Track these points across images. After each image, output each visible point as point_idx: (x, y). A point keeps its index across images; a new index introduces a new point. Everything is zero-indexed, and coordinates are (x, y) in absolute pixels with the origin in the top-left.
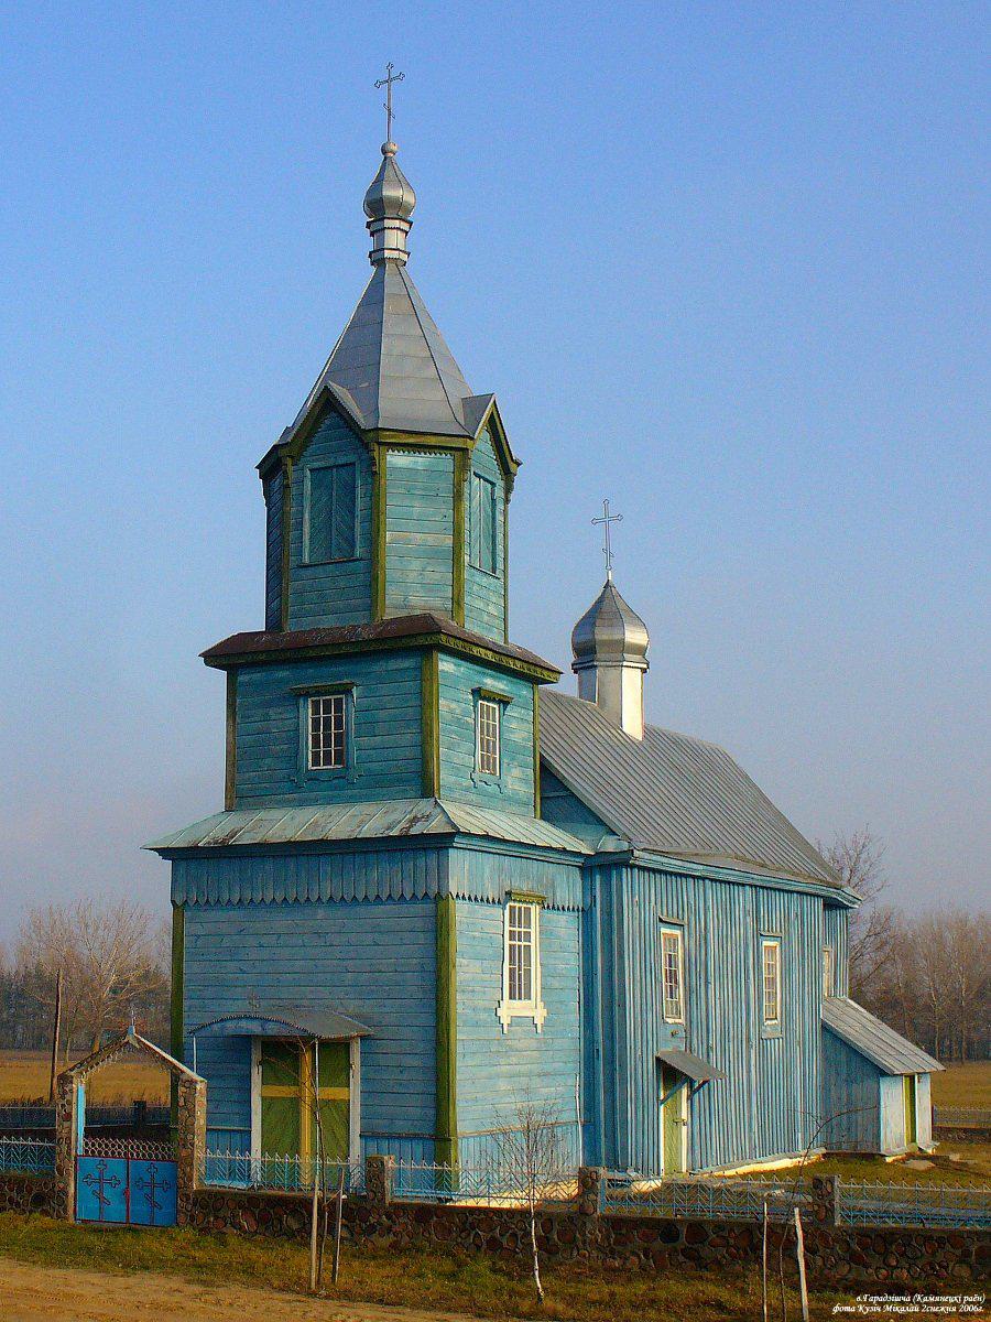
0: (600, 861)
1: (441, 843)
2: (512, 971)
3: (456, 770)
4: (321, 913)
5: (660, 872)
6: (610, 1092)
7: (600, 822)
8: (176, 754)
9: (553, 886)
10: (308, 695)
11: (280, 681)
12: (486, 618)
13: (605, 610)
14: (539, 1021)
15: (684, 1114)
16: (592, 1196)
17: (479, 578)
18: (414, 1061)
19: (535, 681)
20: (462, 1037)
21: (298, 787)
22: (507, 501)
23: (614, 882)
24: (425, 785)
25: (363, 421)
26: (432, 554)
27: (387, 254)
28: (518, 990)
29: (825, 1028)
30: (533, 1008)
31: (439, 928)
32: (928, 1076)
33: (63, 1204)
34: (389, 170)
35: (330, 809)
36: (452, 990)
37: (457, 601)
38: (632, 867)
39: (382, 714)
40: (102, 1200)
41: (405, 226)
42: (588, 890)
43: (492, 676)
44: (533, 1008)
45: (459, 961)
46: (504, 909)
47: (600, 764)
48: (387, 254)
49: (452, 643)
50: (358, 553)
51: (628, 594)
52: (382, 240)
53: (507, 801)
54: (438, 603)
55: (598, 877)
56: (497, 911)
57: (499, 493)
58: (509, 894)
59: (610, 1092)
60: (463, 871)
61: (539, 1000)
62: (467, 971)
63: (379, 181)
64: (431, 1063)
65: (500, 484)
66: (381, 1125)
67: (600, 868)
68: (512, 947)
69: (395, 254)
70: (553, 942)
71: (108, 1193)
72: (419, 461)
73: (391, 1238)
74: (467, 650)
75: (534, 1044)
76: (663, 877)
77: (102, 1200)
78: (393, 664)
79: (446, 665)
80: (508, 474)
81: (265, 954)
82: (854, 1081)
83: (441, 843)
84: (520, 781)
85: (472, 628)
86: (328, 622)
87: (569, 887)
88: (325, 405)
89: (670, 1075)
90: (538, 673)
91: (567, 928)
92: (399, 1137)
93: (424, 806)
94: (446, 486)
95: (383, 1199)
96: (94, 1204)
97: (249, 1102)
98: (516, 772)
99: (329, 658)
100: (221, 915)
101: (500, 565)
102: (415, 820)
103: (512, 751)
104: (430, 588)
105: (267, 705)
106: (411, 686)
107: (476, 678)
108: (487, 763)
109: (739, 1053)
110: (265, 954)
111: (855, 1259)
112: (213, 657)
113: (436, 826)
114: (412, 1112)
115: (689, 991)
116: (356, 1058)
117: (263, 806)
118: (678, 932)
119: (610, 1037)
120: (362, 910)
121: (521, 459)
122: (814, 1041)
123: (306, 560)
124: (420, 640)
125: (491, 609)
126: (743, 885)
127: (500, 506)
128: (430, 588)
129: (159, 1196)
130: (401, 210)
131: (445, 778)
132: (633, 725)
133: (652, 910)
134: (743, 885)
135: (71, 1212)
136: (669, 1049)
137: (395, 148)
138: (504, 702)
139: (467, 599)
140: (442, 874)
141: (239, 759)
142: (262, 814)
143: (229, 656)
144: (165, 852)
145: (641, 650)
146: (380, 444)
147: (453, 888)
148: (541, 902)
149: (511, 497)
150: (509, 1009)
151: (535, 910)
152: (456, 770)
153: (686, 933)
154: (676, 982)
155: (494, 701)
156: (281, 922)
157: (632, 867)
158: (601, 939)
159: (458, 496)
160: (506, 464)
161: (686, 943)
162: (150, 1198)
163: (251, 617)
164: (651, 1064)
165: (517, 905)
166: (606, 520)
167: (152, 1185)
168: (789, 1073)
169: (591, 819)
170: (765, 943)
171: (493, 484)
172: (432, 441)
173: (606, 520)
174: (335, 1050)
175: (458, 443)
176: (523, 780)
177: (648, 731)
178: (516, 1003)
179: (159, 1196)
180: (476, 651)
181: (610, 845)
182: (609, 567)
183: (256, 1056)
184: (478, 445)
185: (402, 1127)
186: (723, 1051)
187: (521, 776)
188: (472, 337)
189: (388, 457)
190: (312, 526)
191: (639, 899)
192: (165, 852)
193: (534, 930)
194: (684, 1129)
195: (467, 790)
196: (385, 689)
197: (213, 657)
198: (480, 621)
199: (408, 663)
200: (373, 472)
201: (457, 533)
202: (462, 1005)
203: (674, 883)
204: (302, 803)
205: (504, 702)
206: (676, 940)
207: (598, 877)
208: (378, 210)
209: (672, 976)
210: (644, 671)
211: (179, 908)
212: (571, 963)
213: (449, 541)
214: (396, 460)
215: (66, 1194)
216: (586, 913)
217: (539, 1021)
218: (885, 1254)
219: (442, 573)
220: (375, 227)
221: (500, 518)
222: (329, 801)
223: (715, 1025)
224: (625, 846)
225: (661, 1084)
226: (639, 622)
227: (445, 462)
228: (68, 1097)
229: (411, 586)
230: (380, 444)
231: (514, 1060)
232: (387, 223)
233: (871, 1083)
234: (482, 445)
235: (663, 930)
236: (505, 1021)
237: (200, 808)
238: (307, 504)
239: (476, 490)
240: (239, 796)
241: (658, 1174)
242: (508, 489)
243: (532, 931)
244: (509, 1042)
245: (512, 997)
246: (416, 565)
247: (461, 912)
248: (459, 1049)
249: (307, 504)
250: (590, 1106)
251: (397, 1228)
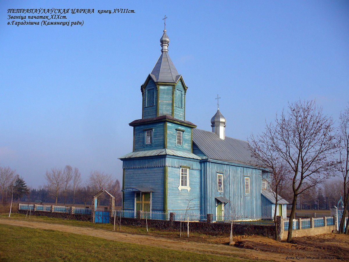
0: (203, 161)
1: (164, 156)
2: (182, 181)
3: (171, 143)
4: (146, 170)
5: (217, 163)
6: (205, 204)
7: (204, 154)
8: (125, 143)
9: (192, 165)
10: (146, 131)
11: (142, 128)
12: (179, 116)
13: (217, 115)
14: (189, 190)
15: (223, 209)
16: (172, 218)
17: (178, 109)
18: (160, 196)
19: (193, 128)
20: (169, 192)
21: (145, 147)
22: (185, 94)
23: (206, 165)
24: (164, 146)
25: (155, 80)
26: (168, 104)
27: (163, 50)
28: (184, 183)
29: (262, 195)
30: (188, 188)
31: (164, 172)
32: (286, 205)
33: (92, 219)
34: (164, 35)
35: (149, 151)
36: (166, 183)
37: (173, 113)
38: (209, 162)
39: (158, 134)
40: (99, 219)
41: (167, 45)
42: (201, 166)
43: (180, 127)
44: (188, 188)
45: (168, 178)
46: (180, 169)
47: (211, 143)
48: (163, 50)
49: (169, 120)
50: (154, 105)
51: (221, 112)
52: (163, 48)
53: (184, 150)
54: (169, 113)
55: (203, 164)
56: (178, 169)
57: (183, 93)
58: (181, 166)
59: (205, 204)
60: (169, 162)
61: (189, 186)
62: (170, 180)
63: (162, 38)
64: (163, 196)
65: (183, 91)
66: (155, 208)
67: (203, 162)
68: (182, 176)
69: (165, 50)
70: (193, 176)
71: (100, 218)
72: (166, 87)
73: (141, 225)
74: (173, 122)
75: (187, 194)
76: (246, 168)
77: (99, 219)
78: (160, 125)
79: (169, 124)
80: (185, 90)
81: (137, 177)
82: (267, 205)
83: (164, 156)
84: (188, 146)
85: (176, 117)
86: (150, 117)
87: (197, 166)
88: (149, 78)
89: (218, 202)
90: (193, 126)
91: (197, 174)
92: (158, 210)
93: (164, 150)
94: (171, 92)
95: (140, 218)
96: (97, 219)
97: (134, 202)
98: (187, 144)
99: (150, 125)
100: (131, 170)
101: (183, 106)
102: (160, 153)
103: (186, 141)
104: (167, 111)
105: (139, 133)
106: (162, 128)
107: (177, 127)
108: (179, 143)
109: (238, 199)
110: (137, 177)
111: (214, 229)
112: (131, 124)
113: (164, 153)
114: (159, 206)
115: (224, 186)
116: (151, 196)
117: (139, 151)
118: (222, 175)
119: (205, 194)
120: (153, 169)
121: (188, 86)
122: (259, 197)
123: (146, 106)
124: (163, 120)
125: (181, 114)
126: (240, 167)
127: (183, 95)
128: (167, 111)
129: (107, 218)
130: (167, 43)
131: (168, 145)
132: (222, 136)
133: (214, 171)
134: (240, 167)
135: (94, 221)
136: (219, 197)
137: (166, 31)
138: (183, 131)
139: (175, 112)
140: (165, 163)
141: (135, 142)
142: (138, 152)
143: (134, 124)
144: (121, 159)
145: (224, 123)
146: (158, 85)
147: (167, 164)
148: (189, 168)
149: (186, 94)
150: (181, 188)
151: (188, 170)
152: (171, 143)
153: (224, 175)
154: (221, 184)
155: (180, 131)
156: (140, 171)
157: (209, 162)
158: (203, 174)
159: (173, 94)
160: (185, 88)
161: (224, 177)
162: (106, 218)
163: (139, 116)
164: (214, 199)
165: (183, 168)
166: (218, 98)
167: (106, 216)
168: (252, 203)
169: (202, 153)
170: (245, 178)
171: (182, 91)
172: (168, 84)
173: (218, 98)
174: (147, 194)
175: (173, 84)
176: (189, 146)
177: (226, 138)
178: (183, 187)
179: (107, 218)
180: (175, 122)
181: (204, 158)
182: (218, 107)
183: (135, 196)
184: (179, 84)
185: (158, 208)
186: (234, 198)
187: (187, 145)
188: (180, 64)
189: (160, 87)
190: (147, 100)
191: (211, 169)
192: (121, 159)
193: (188, 173)
194: (223, 212)
195: (174, 147)
196: (158, 129)
197: (131, 124)
198: (179, 115)
199: (162, 124)
200: (157, 90)
201: (173, 100)
202: (169, 186)
203: (220, 166)
204: (145, 150)
205: (183, 131)
206: (221, 176)
207: (203, 164)
208: (162, 42)
209: (220, 183)
210: (225, 127)
211: (124, 169)
212: (198, 180)
213: (171, 102)
214: (161, 87)
215: (93, 218)
216: (201, 171)
217: (189, 190)
218: (218, 229)
219: (170, 108)
220: (162, 45)
221: (183, 98)
222: (149, 150)
223: (232, 193)
224: (207, 158)
225: (217, 202)
226: (223, 117)
227: (171, 87)
228: (93, 201)
229: (163, 110)
230: (158, 85)
231: (182, 197)
232: (164, 45)
233: (270, 206)
234: (179, 84)
235: (218, 174)
236: (180, 190)
237: (128, 151)
238: (147, 96)
239: (178, 93)
240: (135, 150)
241: (216, 220)
242: (185, 92)
243: (187, 173)
244: (181, 194)
245: (182, 185)
246: (165, 106)
247: (169, 170)
248: (168, 194)
249: (147, 96)
250: (201, 207)
251: (142, 223)
